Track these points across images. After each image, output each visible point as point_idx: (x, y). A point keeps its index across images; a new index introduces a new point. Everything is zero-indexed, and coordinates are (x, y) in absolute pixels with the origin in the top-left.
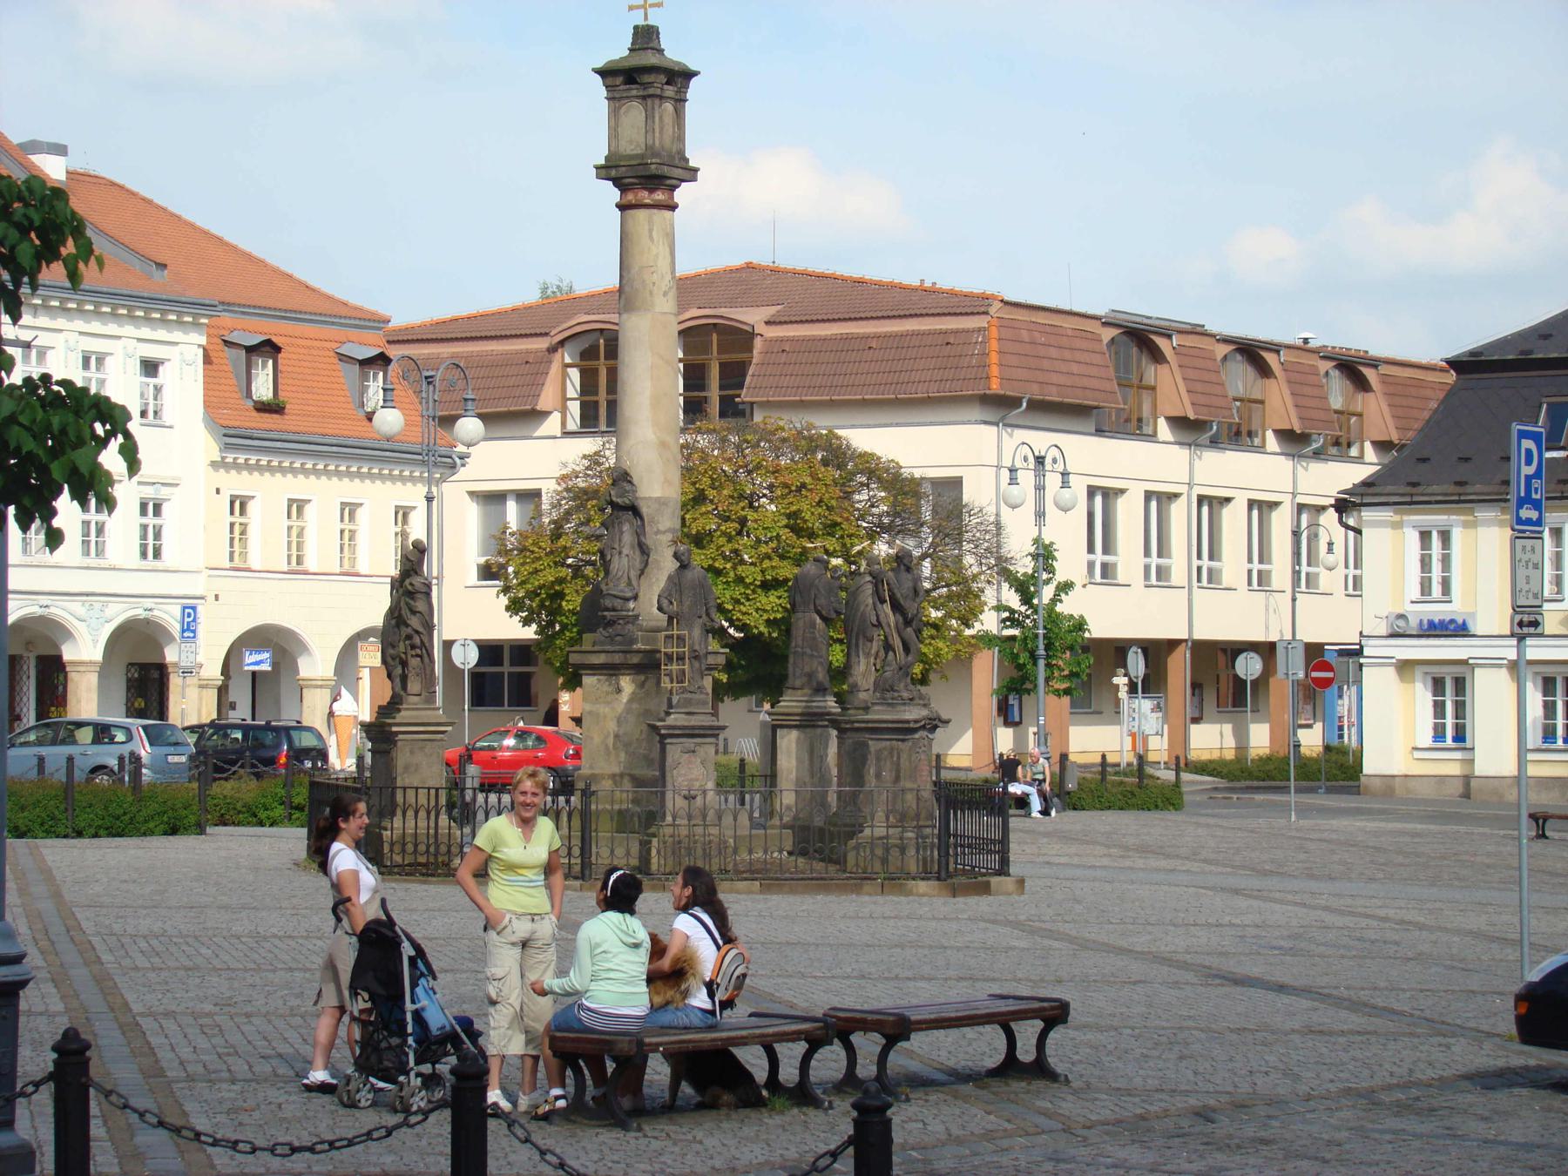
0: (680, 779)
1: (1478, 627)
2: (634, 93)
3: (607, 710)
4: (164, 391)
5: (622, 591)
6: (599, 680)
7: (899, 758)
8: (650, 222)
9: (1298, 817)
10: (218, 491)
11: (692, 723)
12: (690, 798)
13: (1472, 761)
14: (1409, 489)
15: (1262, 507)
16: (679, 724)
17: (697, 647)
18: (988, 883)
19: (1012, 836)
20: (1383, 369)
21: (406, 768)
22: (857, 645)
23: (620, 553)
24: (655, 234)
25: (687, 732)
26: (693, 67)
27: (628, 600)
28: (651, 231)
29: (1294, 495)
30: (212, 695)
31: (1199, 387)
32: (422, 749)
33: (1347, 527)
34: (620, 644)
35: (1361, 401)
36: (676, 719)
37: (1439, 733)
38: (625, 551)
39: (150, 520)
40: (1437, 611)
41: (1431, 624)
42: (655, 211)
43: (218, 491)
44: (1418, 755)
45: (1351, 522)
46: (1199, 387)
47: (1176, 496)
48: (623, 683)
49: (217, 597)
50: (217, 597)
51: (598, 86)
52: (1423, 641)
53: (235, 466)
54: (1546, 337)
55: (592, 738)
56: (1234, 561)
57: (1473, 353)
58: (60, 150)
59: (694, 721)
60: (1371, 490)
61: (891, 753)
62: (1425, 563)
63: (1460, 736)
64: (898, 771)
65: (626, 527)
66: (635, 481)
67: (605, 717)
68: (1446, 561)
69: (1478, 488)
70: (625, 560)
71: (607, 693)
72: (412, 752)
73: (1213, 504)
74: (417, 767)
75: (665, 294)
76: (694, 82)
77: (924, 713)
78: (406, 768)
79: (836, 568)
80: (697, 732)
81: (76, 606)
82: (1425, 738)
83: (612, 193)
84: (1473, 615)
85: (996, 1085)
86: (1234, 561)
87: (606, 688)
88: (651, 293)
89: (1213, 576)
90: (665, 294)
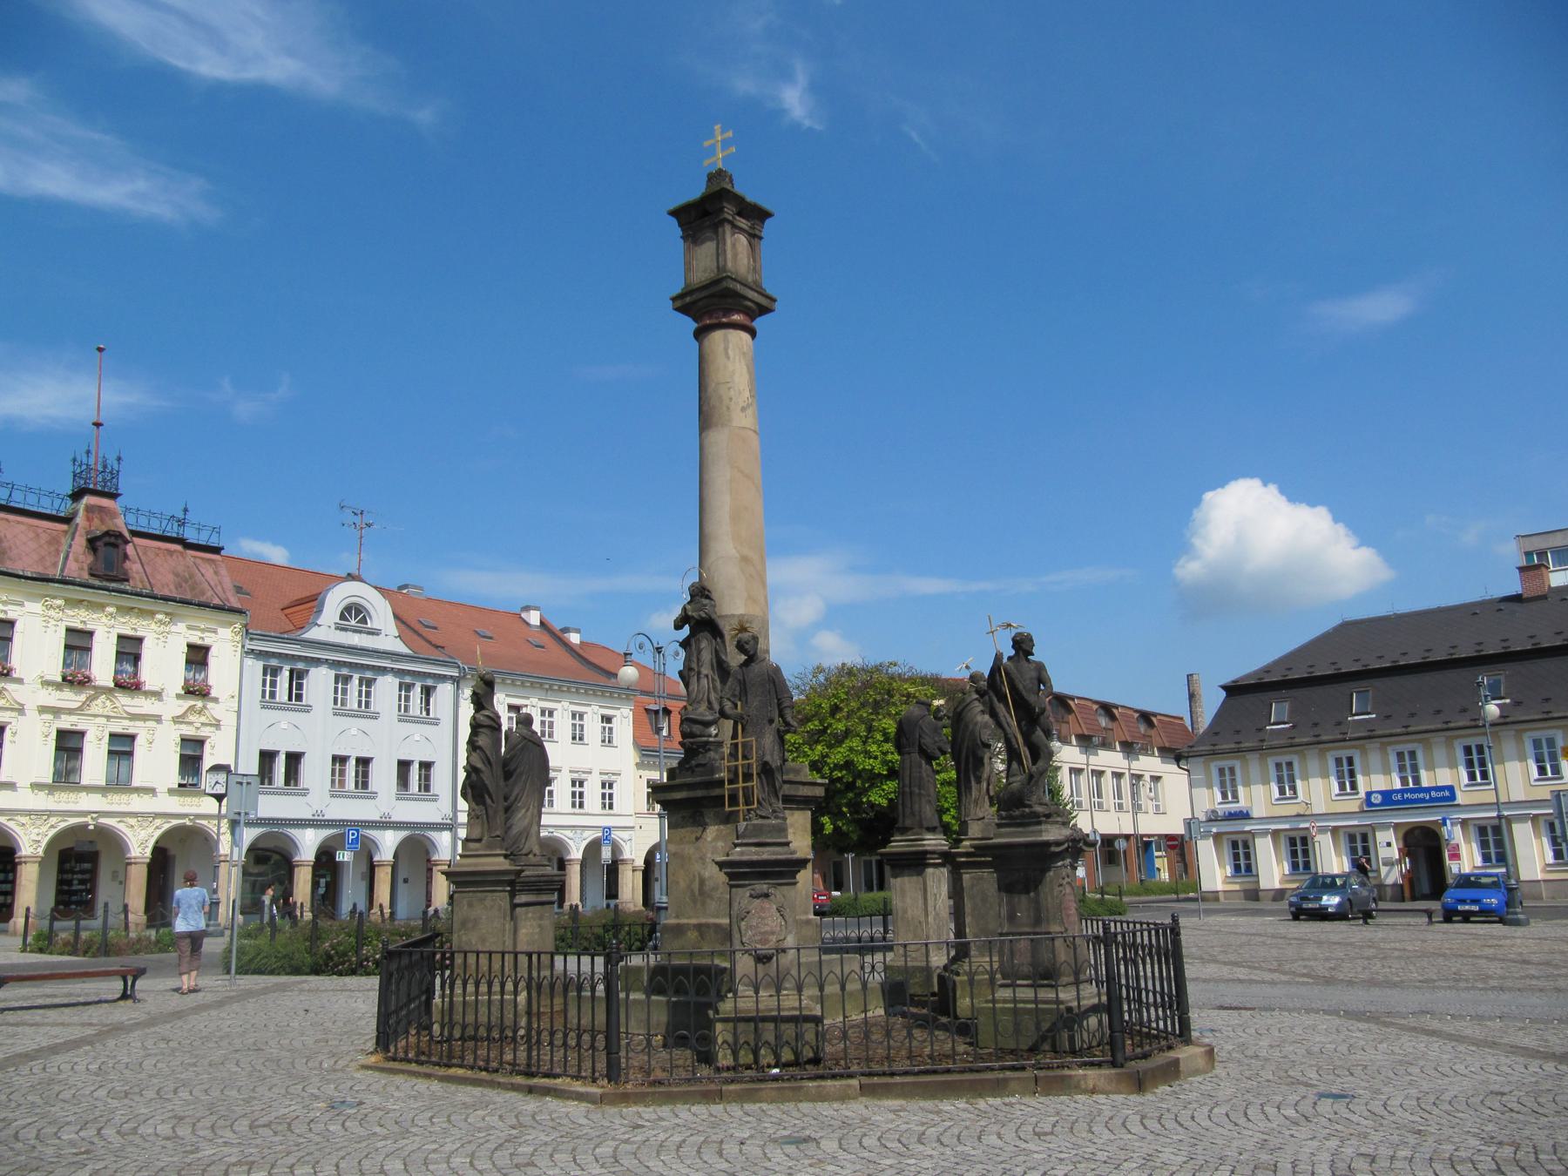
1: (1255, 814)
4: (614, 730)
5: (701, 714)
8: (726, 341)
11: (765, 857)
12: (763, 959)
13: (1258, 881)
15: (1118, 776)
16: (745, 858)
17: (768, 758)
18: (1176, 1062)
19: (1191, 988)
20: (1159, 717)
21: (464, 923)
23: (699, 673)
24: (730, 352)
26: (765, 204)
27: (707, 724)
28: (726, 349)
29: (1129, 769)
30: (639, 875)
31: (1088, 721)
35: (1152, 732)
36: (742, 853)
39: (607, 791)
40: (1233, 807)
41: (1230, 814)
46: (1088, 721)
47: (1082, 770)
51: (673, 228)
52: (1227, 823)
54: (1268, 672)
55: (678, 883)
56: (1109, 799)
58: (578, 631)
63: (1249, 868)
65: (704, 644)
66: (714, 595)
67: (690, 858)
69: (1247, 745)
70: (704, 682)
72: (470, 905)
73: (1099, 774)
76: (768, 222)
77: (1066, 832)
78: (464, 923)
79: (938, 709)
81: (568, 833)
83: (690, 325)
84: (1251, 808)
86: (1109, 799)
88: (728, 408)
89: (1100, 805)
90: (743, 409)
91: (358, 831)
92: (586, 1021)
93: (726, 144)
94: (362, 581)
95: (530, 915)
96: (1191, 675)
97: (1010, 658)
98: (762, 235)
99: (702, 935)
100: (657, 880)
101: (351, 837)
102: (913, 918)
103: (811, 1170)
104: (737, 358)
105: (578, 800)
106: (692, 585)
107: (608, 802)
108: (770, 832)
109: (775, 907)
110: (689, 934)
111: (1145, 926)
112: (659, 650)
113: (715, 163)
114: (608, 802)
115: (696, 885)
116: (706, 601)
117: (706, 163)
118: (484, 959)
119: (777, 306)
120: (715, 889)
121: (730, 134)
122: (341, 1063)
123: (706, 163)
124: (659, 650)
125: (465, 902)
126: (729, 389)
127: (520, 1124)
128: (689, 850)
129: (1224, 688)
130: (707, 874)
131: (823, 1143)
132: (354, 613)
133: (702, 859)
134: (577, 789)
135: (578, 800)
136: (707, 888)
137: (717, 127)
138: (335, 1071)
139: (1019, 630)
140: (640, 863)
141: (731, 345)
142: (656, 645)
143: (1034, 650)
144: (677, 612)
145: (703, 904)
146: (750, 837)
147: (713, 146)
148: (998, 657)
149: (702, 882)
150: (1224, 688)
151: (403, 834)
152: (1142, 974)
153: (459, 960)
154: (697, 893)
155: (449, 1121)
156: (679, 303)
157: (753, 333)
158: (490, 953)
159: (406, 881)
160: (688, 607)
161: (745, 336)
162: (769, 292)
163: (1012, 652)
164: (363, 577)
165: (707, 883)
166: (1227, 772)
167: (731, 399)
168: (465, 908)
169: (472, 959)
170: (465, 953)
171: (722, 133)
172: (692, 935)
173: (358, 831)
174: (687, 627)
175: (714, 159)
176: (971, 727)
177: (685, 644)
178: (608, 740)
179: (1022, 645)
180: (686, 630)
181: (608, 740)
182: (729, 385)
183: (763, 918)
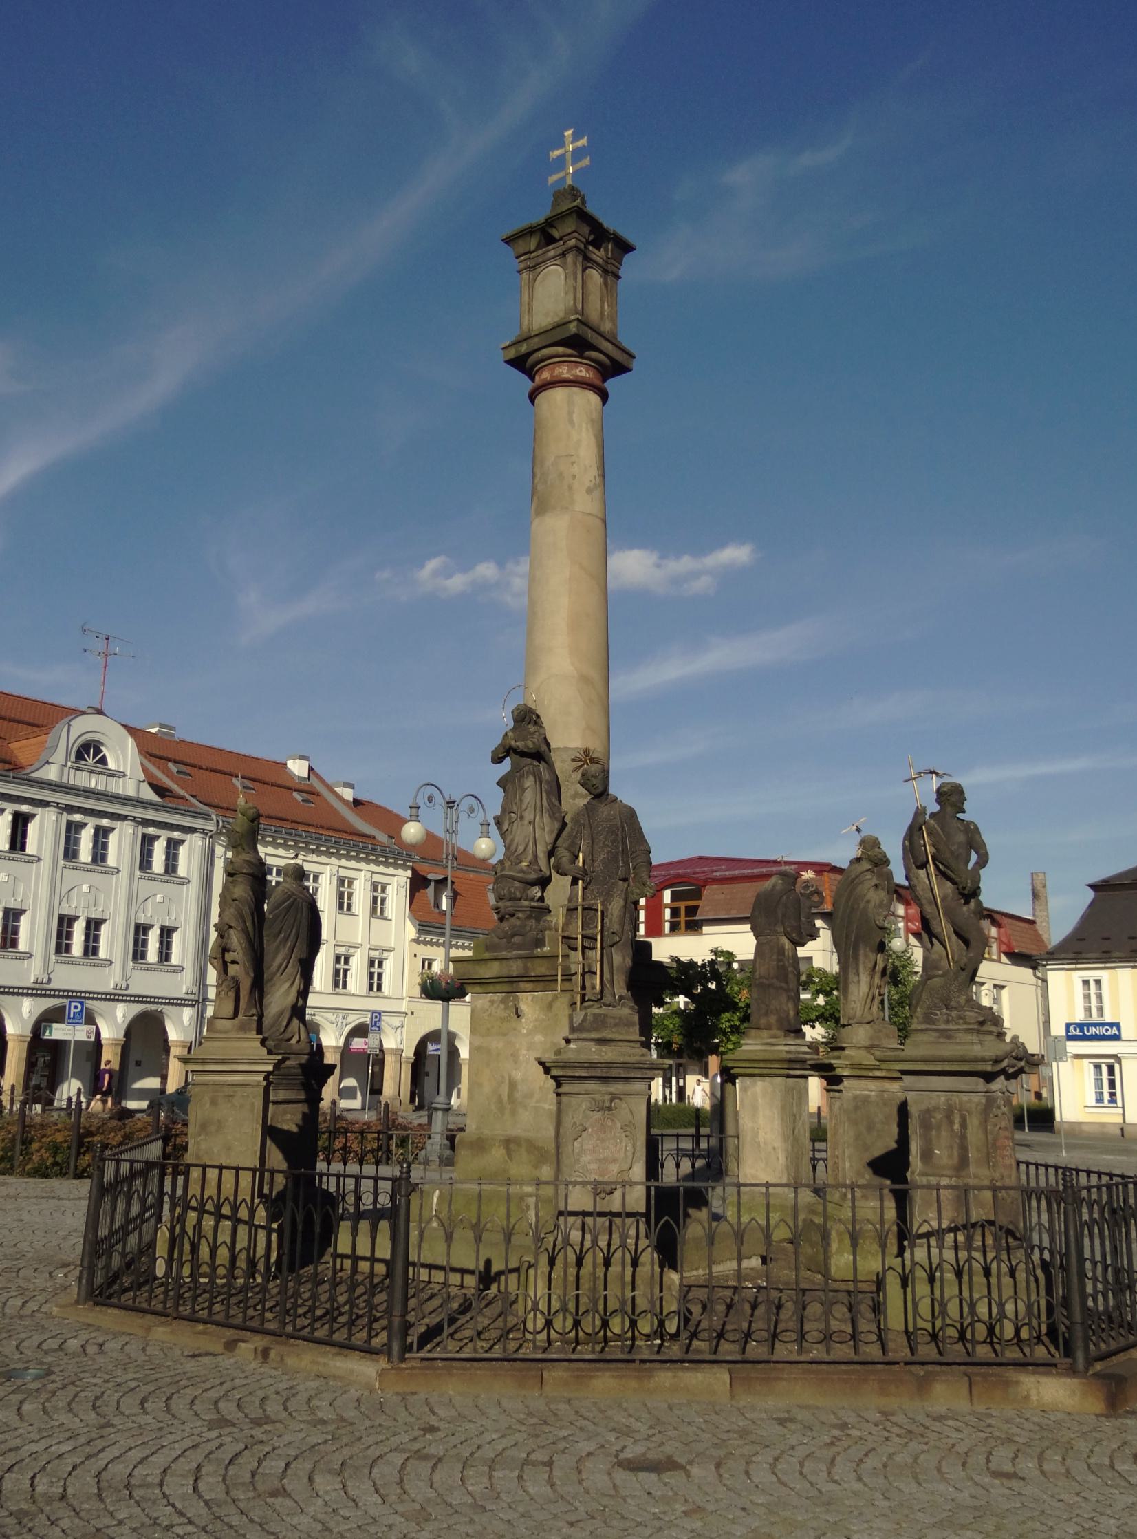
0: (585, 1159)
2: (551, 254)
3: (501, 1045)
6: (492, 1002)
7: (964, 1125)
9: (1066, 1152)
10: (415, 955)
14: (1075, 956)
16: (583, 1058)
21: (204, 1127)
22: (856, 958)
23: (522, 818)
25: (598, 1073)
28: (570, 413)
32: (230, 1097)
33: (1038, 978)
34: (520, 947)
37: (1100, 1099)
38: (529, 816)
42: (576, 390)
43: (415, 955)
44: (1088, 1110)
45: (1039, 975)
48: (523, 1007)
49: (412, 1013)
50: (412, 1013)
53: (425, 943)
57: (1104, 881)
58: (351, 786)
59: (609, 1054)
60: (1052, 957)
61: (949, 1116)
62: (1087, 997)
64: (964, 1148)
68: (1099, 997)
71: (503, 1020)
72: (214, 1102)
74: (220, 1125)
75: (589, 491)
76: (628, 258)
78: (204, 1127)
80: (614, 1073)
82: (1091, 1099)
85: (740, 1161)
87: (500, 1011)
88: (570, 488)
91: (82, 1003)
92: (363, 1249)
93: (578, 154)
94: (105, 715)
95: (288, 1116)
96: (1036, 874)
97: (933, 815)
98: (621, 273)
99: (509, 1153)
100: (427, 1074)
101: (73, 1010)
102: (765, 1143)
103: (690, 1524)
104: (584, 425)
105: (340, 979)
106: (517, 708)
107: (374, 983)
108: (615, 1025)
109: (619, 1125)
110: (494, 1152)
111: (1105, 1179)
112: (451, 804)
113: (563, 179)
114: (374, 983)
115: (505, 1090)
116: (532, 728)
117: (553, 179)
118: (228, 1176)
119: (635, 364)
120: (530, 1095)
121: (583, 142)
122: (32, 1306)
123: (553, 179)
124: (451, 804)
125: (207, 1099)
126: (573, 463)
127: (267, 1417)
128: (496, 1044)
129: (1093, 887)
130: (518, 1076)
131: (695, 1470)
132: (89, 750)
133: (514, 1056)
134: (342, 966)
135: (340, 979)
136: (518, 1095)
137: (569, 133)
138: (21, 1317)
139: (946, 779)
140: (409, 1053)
141: (576, 410)
142: (448, 799)
143: (966, 806)
144: (496, 741)
145: (513, 1113)
146: (589, 1031)
147: (562, 158)
148: (920, 812)
149: (513, 1086)
150: (1093, 887)
151: (137, 1009)
152: (1107, 1244)
153: (195, 1173)
154: (505, 1098)
155: (168, 1409)
156: (512, 354)
157: (604, 396)
158: (238, 1169)
159: (138, 1064)
160: (510, 734)
161: (594, 398)
162: (626, 344)
163: (936, 808)
164: (105, 712)
165: (519, 1087)
166: (1092, 984)
167: (574, 477)
168: (208, 1105)
169: (212, 1174)
170: (205, 1167)
171: (574, 141)
172: (498, 1153)
173: (82, 1003)
174: (508, 760)
175: (561, 174)
176: (862, 905)
177: (502, 783)
178: (377, 907)
179: (951, 797)
180: (507, 765)
181: (377, 907)
182: (573, 459)
183: (603, 1141)
